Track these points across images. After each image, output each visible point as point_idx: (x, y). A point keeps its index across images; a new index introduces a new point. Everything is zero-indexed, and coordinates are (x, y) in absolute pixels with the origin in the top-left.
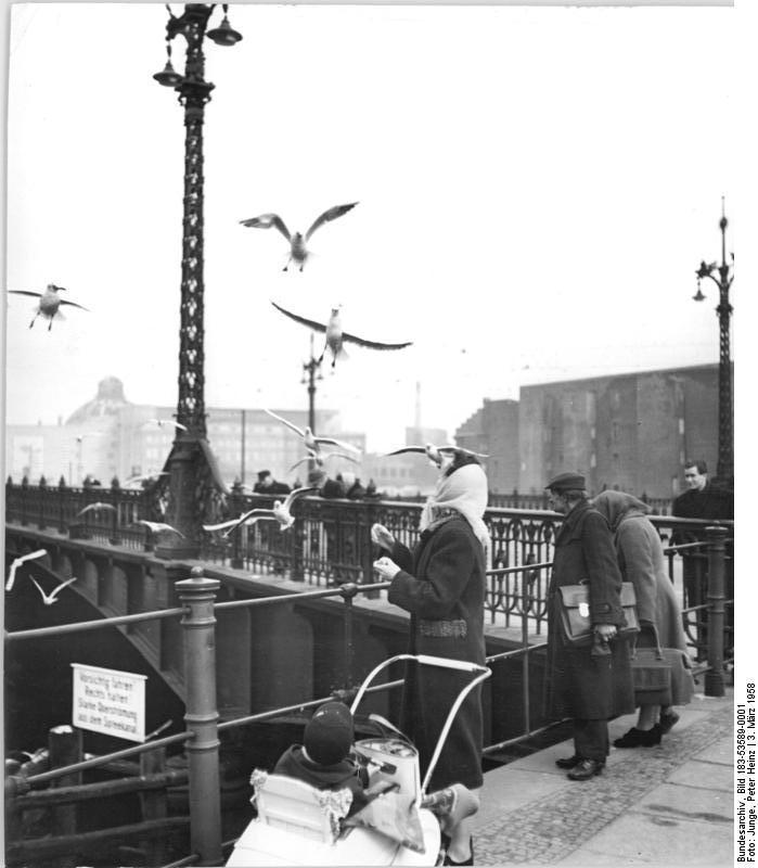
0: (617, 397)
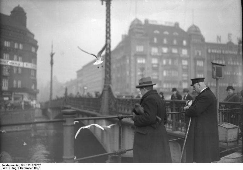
0: (9, 67)
